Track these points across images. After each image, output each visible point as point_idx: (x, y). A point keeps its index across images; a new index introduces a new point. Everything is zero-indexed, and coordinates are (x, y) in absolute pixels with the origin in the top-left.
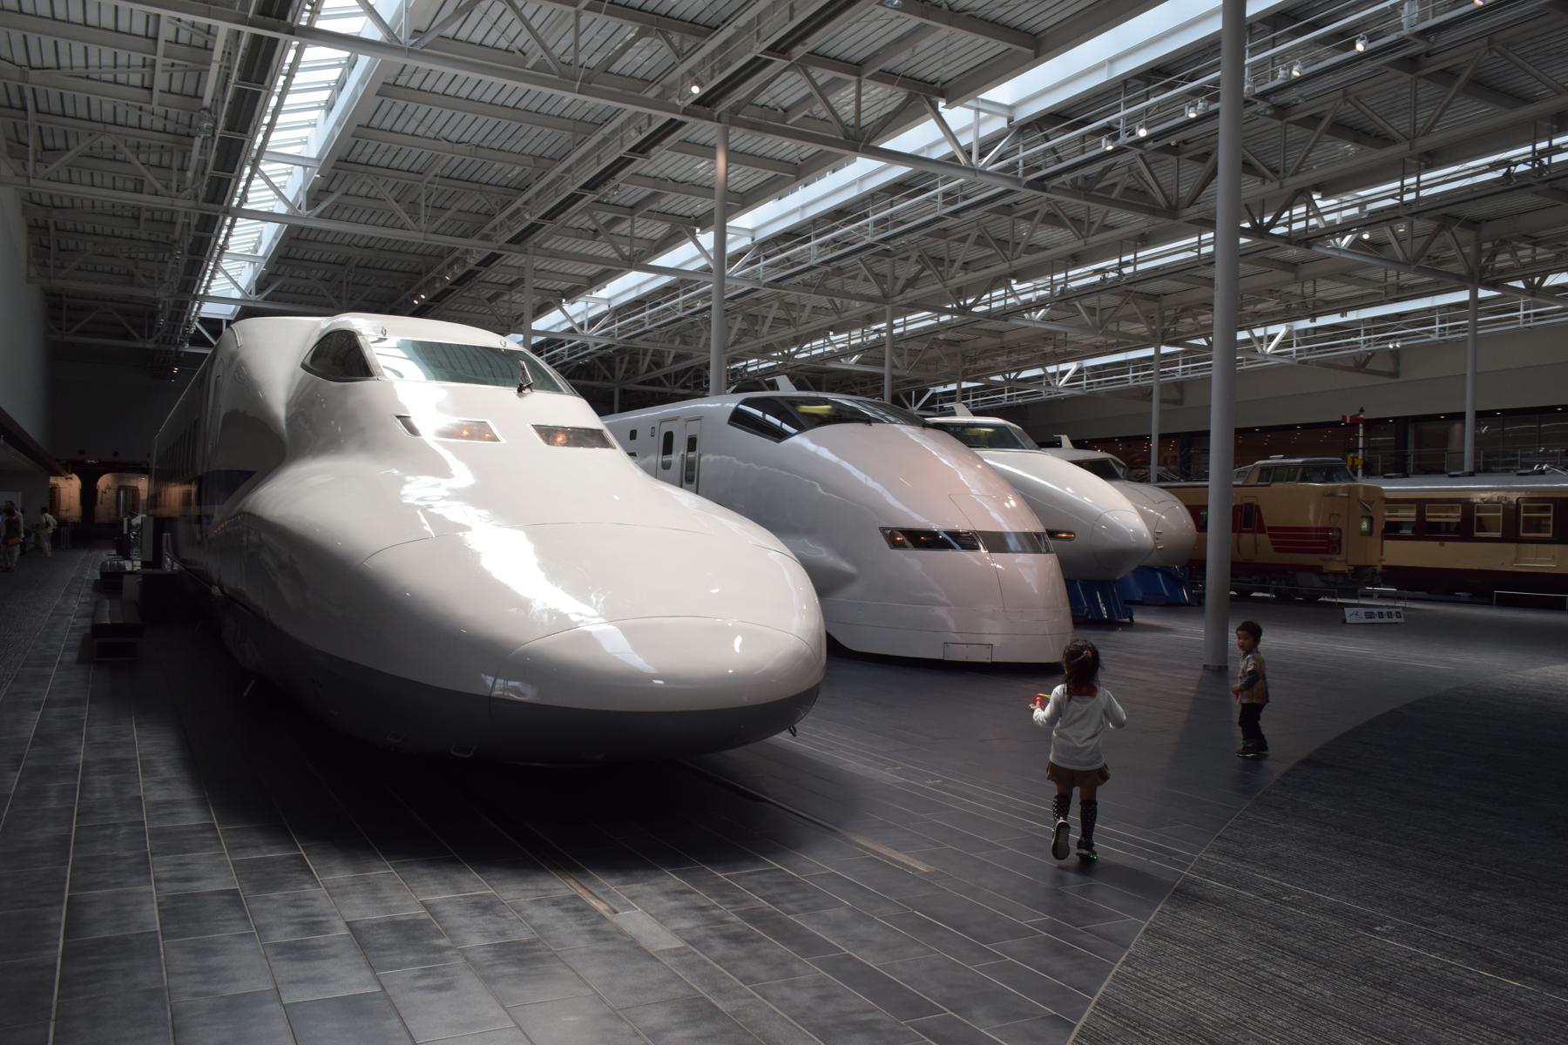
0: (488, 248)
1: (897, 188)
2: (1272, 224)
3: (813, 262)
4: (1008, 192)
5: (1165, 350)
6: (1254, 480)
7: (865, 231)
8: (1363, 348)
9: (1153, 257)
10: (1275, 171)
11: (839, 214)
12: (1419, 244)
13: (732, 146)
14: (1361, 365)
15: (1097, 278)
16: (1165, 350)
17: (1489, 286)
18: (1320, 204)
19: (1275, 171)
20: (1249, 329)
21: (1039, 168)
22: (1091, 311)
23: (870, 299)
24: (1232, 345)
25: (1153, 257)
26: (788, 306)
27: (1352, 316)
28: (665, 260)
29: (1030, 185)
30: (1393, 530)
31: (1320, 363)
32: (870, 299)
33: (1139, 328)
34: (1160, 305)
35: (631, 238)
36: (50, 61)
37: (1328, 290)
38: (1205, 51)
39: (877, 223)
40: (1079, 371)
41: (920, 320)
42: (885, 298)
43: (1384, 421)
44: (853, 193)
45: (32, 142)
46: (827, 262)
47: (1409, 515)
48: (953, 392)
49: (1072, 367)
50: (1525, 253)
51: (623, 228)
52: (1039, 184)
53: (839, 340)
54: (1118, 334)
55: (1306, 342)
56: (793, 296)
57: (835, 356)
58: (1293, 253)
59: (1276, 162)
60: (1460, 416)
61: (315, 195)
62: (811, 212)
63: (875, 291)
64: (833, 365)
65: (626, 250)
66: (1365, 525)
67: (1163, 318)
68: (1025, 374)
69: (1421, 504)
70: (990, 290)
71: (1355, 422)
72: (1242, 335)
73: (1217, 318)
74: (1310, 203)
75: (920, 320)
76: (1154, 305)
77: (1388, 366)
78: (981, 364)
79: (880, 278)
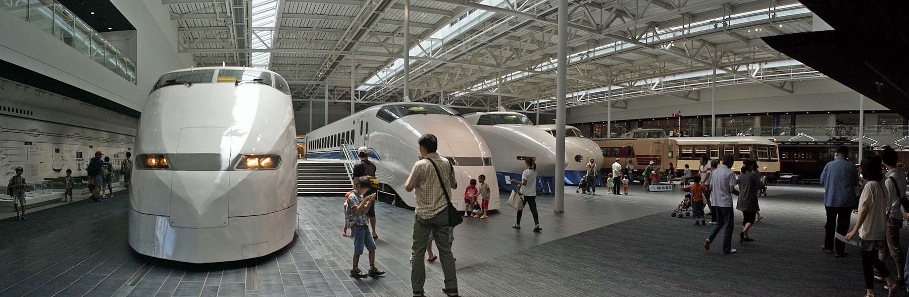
0: (339, 53)
1: (493, 20)
2: (639, 39)
3: (464, 51)
4: (531, 21)
5: (613, 88)
6: (631, 137)
7: (481, 37)
8: (792, 78)
9: (601, 51)
10: (634, 16)
11: (473, 31)
12: (695, 51)
13: (412, 4)
14: (686, 96)
15: (712, 27)
16: (613, 88)
17: (721, 68)
18: (658, 32)
19: (634, 16)
20: (571, 92)
21: (542, 11)
22: (583, 71)
23: (492, 66)
24: (564, 99)
25: (601, 51)
26: (463, 69)
27: (678, 77)
28: (369, 81)
29: (539, 18)
30: (683, 156)
31: (672, 94)
32: (492, 66)
33: (603, 78)
34: (609, 70)
35: (393, 45)
36: (187, 11)
37: (669, 66)
38: (402, 72)
39: (486, 34)
40: (586, 95)
41: (517, 75)
42: (498, 65)
43: (784, 113)
44: (476, 23)
45: (185, 25)
46: (470, 51)
47: (690, 151)
48: (607, 92)
49: (583, 93)
50: (629, 76)
51: (390, 41)
52: (543, 17)
53: (488, 83)
54: (596, 81)
55: (765, 74)
56: (465, 66)
57: (487, 90)
58: (650, 50)
59: (635, 12)
60: (711, 116)
61: (277, 40)
62: (463, 31)
63: (494, 63)
64: (486, 93)
65: (391, 50)
66: (670, 154)
67: (612, 75)
68: (637, 84)
69: (694, 146)
70: (541, 62)
71: (677, 118)
72: (568, 96)
73: (558, 90)
74: (654, 31)
75: (517, 75)
76: (608, 69)
77: (696, 97)
78: (547, 92)
79: (495, 58)
